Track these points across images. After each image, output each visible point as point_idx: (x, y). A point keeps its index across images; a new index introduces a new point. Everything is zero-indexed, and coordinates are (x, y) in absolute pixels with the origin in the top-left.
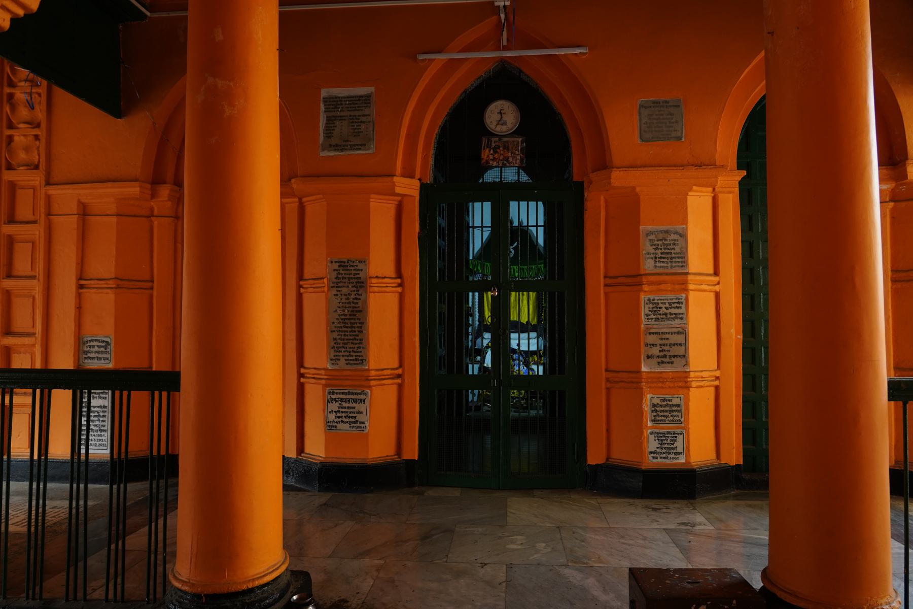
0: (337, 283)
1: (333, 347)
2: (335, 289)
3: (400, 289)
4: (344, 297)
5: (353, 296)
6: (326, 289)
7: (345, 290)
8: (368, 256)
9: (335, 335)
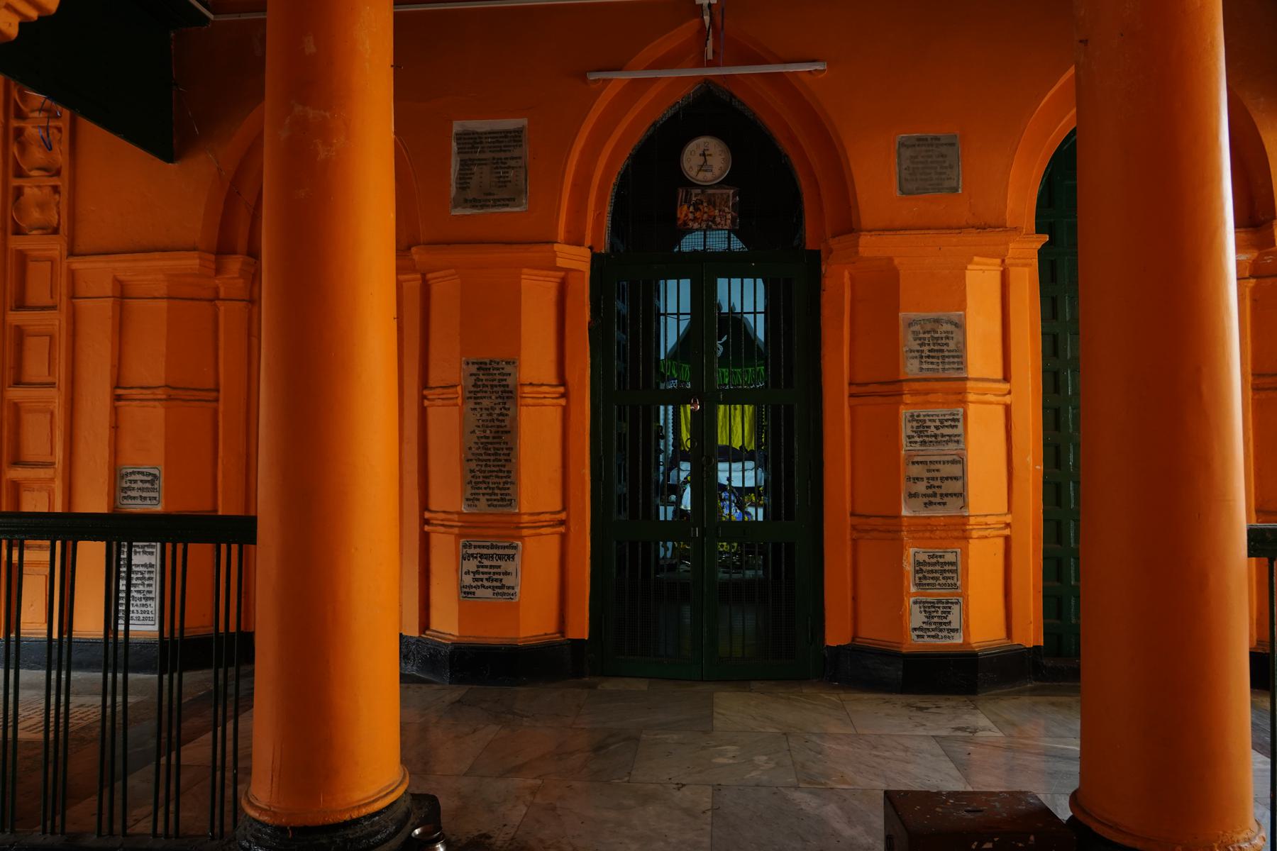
3: (563, 402)
4: (484, 412)
5: (497, 411)
6: (459, 401)
7: (486, 403)
9: (473, 465)
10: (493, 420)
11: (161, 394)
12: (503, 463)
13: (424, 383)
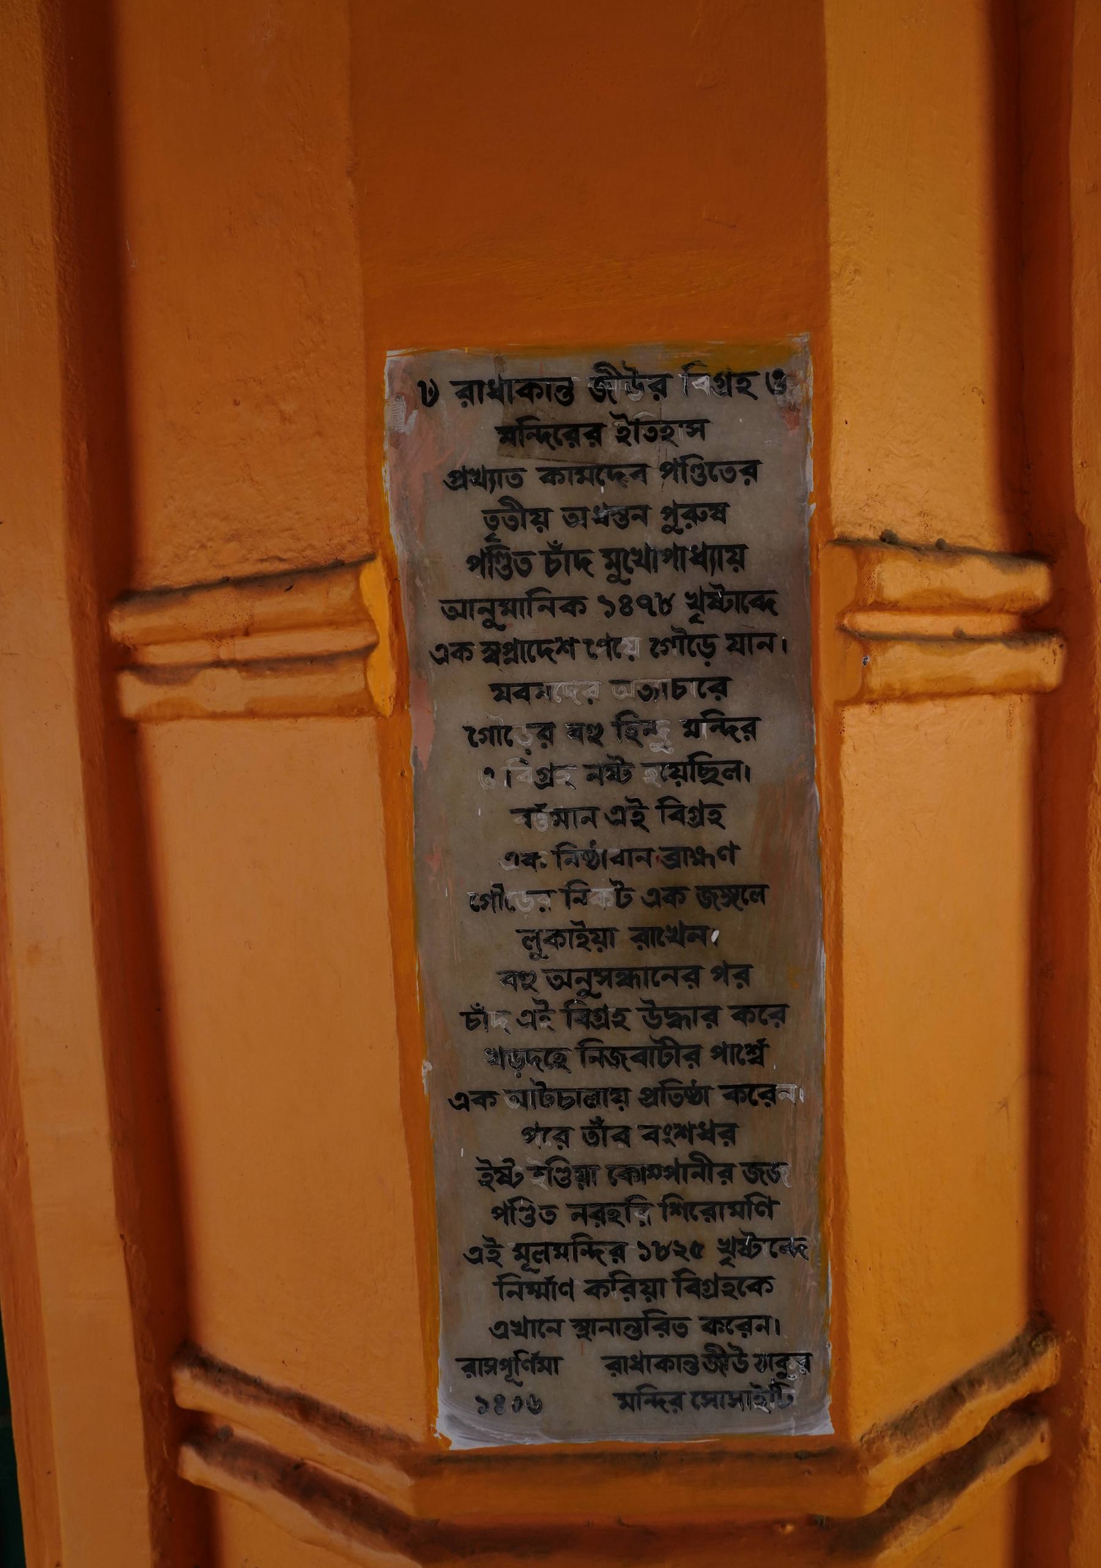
0: (492, 610)
1: (485, 1252)
2: (478, 674)
3: (1044, 662)
4: (564, 749)
5: (665, 745)
6: (381, 676)
7: (577, 686)
8: (817, 319)
9: (501, 1132)
10: (632, 813)
11: (1000, 623)
12: (719, 1108)
13: (112, 566)
